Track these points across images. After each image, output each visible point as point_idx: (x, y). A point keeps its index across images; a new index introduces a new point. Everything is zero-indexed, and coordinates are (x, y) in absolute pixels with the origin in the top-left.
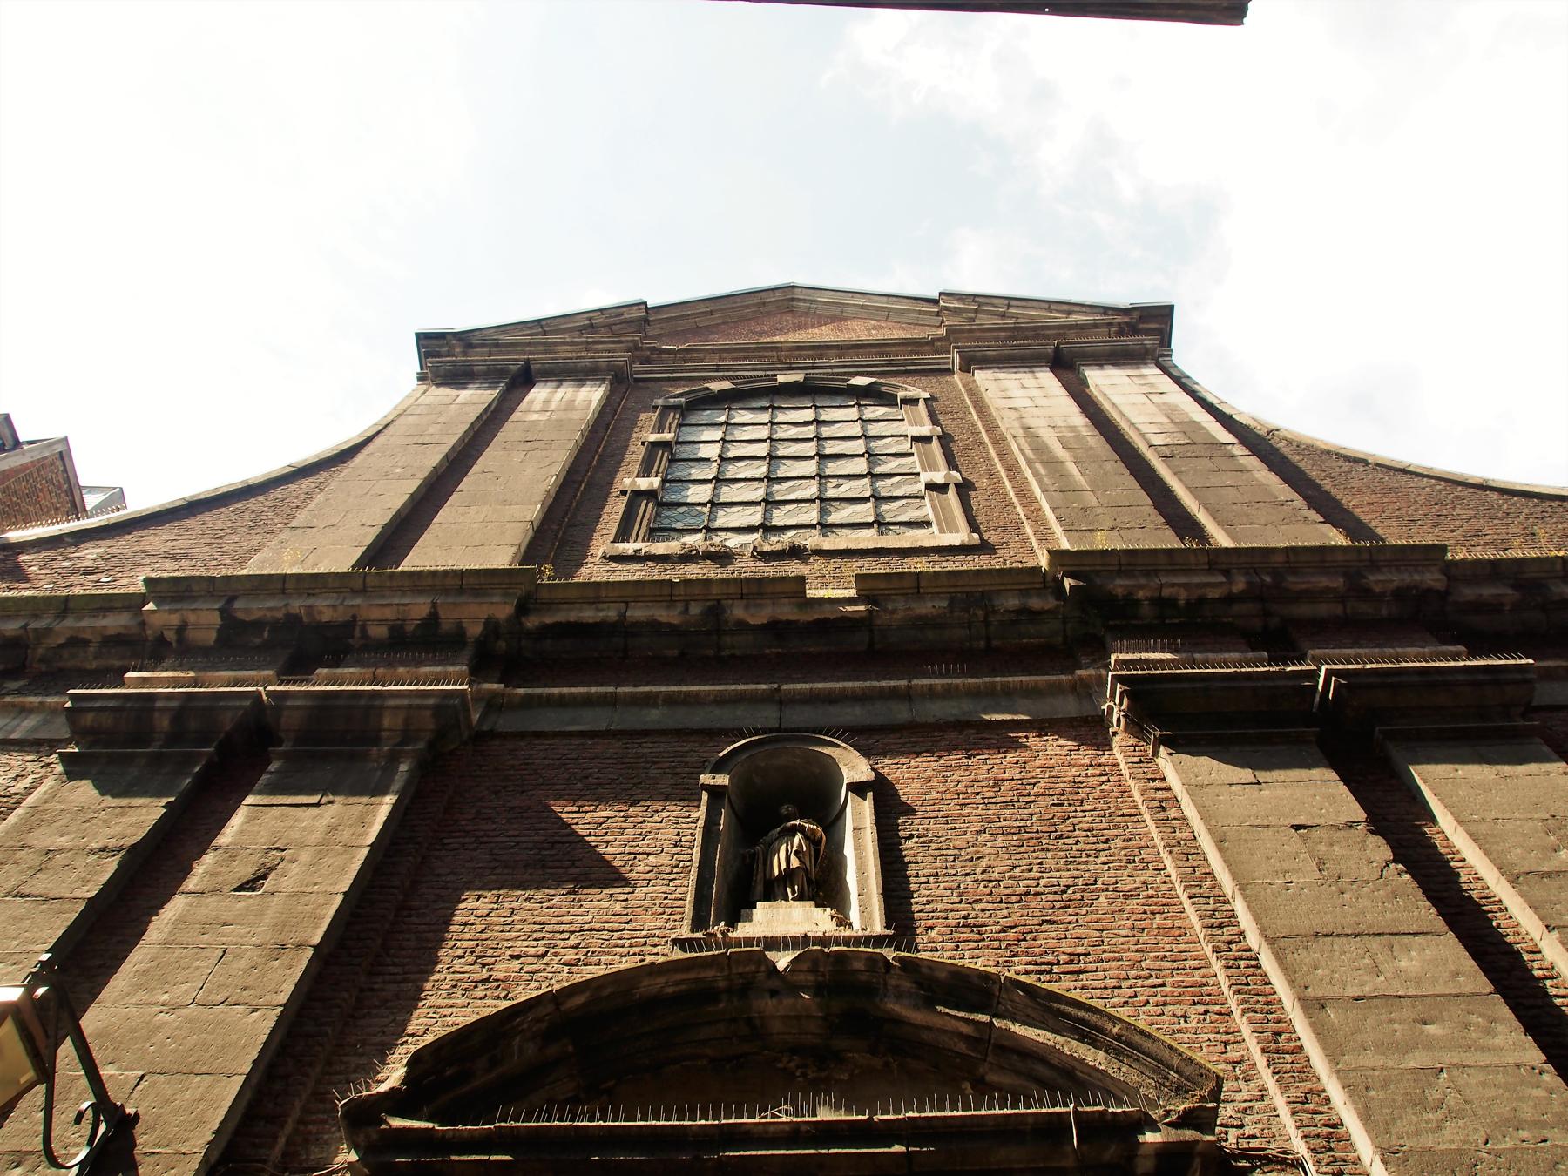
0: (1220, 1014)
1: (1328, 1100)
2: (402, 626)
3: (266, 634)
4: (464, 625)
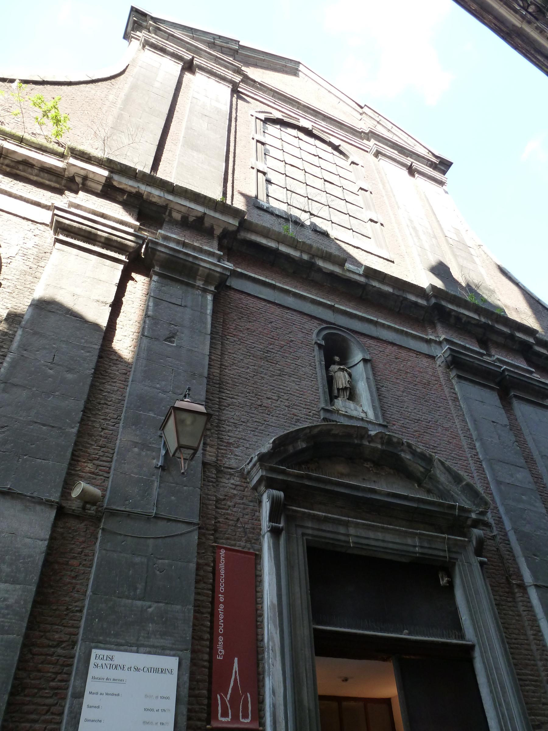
0: (471, 477)
1: (498, 511)
2: (187, 218)
3: (125, 197)
4: (214, 227)
